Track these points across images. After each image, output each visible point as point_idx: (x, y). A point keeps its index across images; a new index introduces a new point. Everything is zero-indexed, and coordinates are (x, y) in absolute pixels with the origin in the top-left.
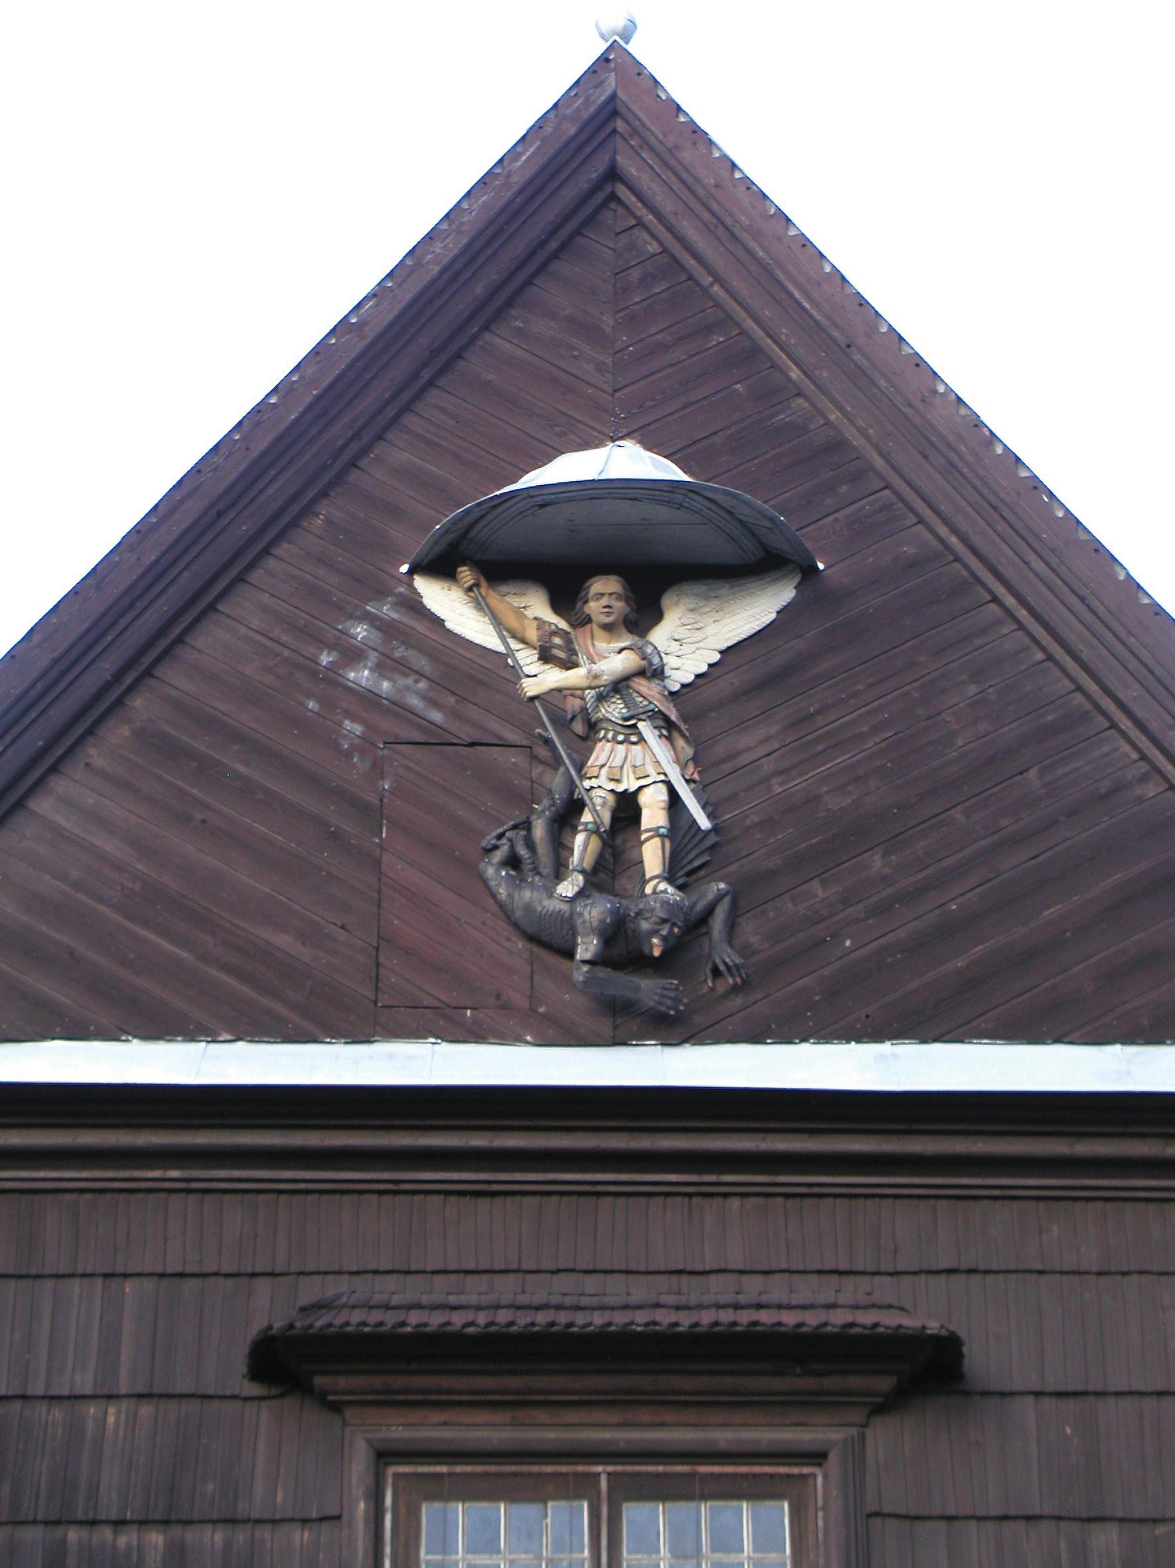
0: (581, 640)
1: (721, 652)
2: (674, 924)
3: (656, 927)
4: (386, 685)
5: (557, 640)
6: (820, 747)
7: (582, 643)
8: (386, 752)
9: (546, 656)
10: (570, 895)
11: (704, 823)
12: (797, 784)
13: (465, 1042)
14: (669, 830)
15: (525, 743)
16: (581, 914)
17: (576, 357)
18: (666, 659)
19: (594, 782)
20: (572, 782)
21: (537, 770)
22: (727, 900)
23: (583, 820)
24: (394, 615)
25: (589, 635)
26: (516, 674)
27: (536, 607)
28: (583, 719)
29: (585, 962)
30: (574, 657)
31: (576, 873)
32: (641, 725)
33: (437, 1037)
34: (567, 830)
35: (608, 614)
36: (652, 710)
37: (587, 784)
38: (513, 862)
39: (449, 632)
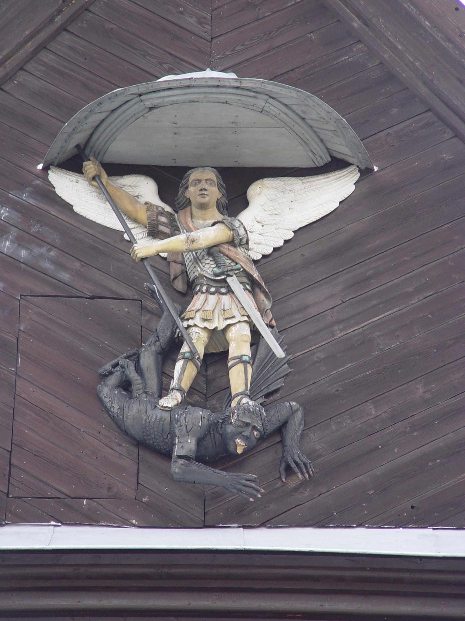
0: (182, 219)
1: (294, 232)
2: (254, 428)
4: (23, 253)
5: (163, 219)
6: (374, 302)
7: (183, 221)
8: (23, 302)
11: (279, 352)
12: (354, 330)
13: (81, 524)
15: (136, 297)
16: (178, 420)
17: (181, 13)
18: (250, 236)
19: (191, 322)
20: (174, 323)
21: (146, 318)
23: (182, 351)
24: (31, 201)
27: (145, 190)
28: (183, 279)
29: (180, 457)
31: (175, 391)
32: (229, 280)
33: (58, 521)
34: (170, 362)
36: (239, 269)
37: (185, 324)
38: (126, 385)
39: (76, 213)
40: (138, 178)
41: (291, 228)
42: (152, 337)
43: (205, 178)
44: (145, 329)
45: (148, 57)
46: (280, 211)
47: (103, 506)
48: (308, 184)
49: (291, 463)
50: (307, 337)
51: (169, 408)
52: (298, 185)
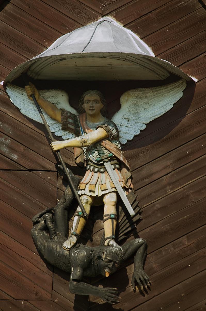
2: (115, 262)
3: (107, 264)
5: (70, 120)
6: (191, 171)
7: (81, 123)
9: (65, 128)
10: (69, 247)
12: (178, 189)
14: (115, 215)
18: (120, 129)
19: (83, 192)
22: (142, 247)
25: (84, 119)
26: (51, 137)
27: (62, 101)
29: (74, 280)
30: (78, 128)
31: (73, 236)
32: (105, 164)
35: (92, 110)
37: (80, 193)
38: (46, 228)
40: (57, 92)
41: (145, 122)
42: (62, 199)
43: (93, 100)
44: (59, 190)
45: (66, 5)
46: (139, 111)
47: (33, 305)
48: (156, 93)
49: (137, 280)
50: (151, 194)
51: (69, 249)
52: (150, 93)
